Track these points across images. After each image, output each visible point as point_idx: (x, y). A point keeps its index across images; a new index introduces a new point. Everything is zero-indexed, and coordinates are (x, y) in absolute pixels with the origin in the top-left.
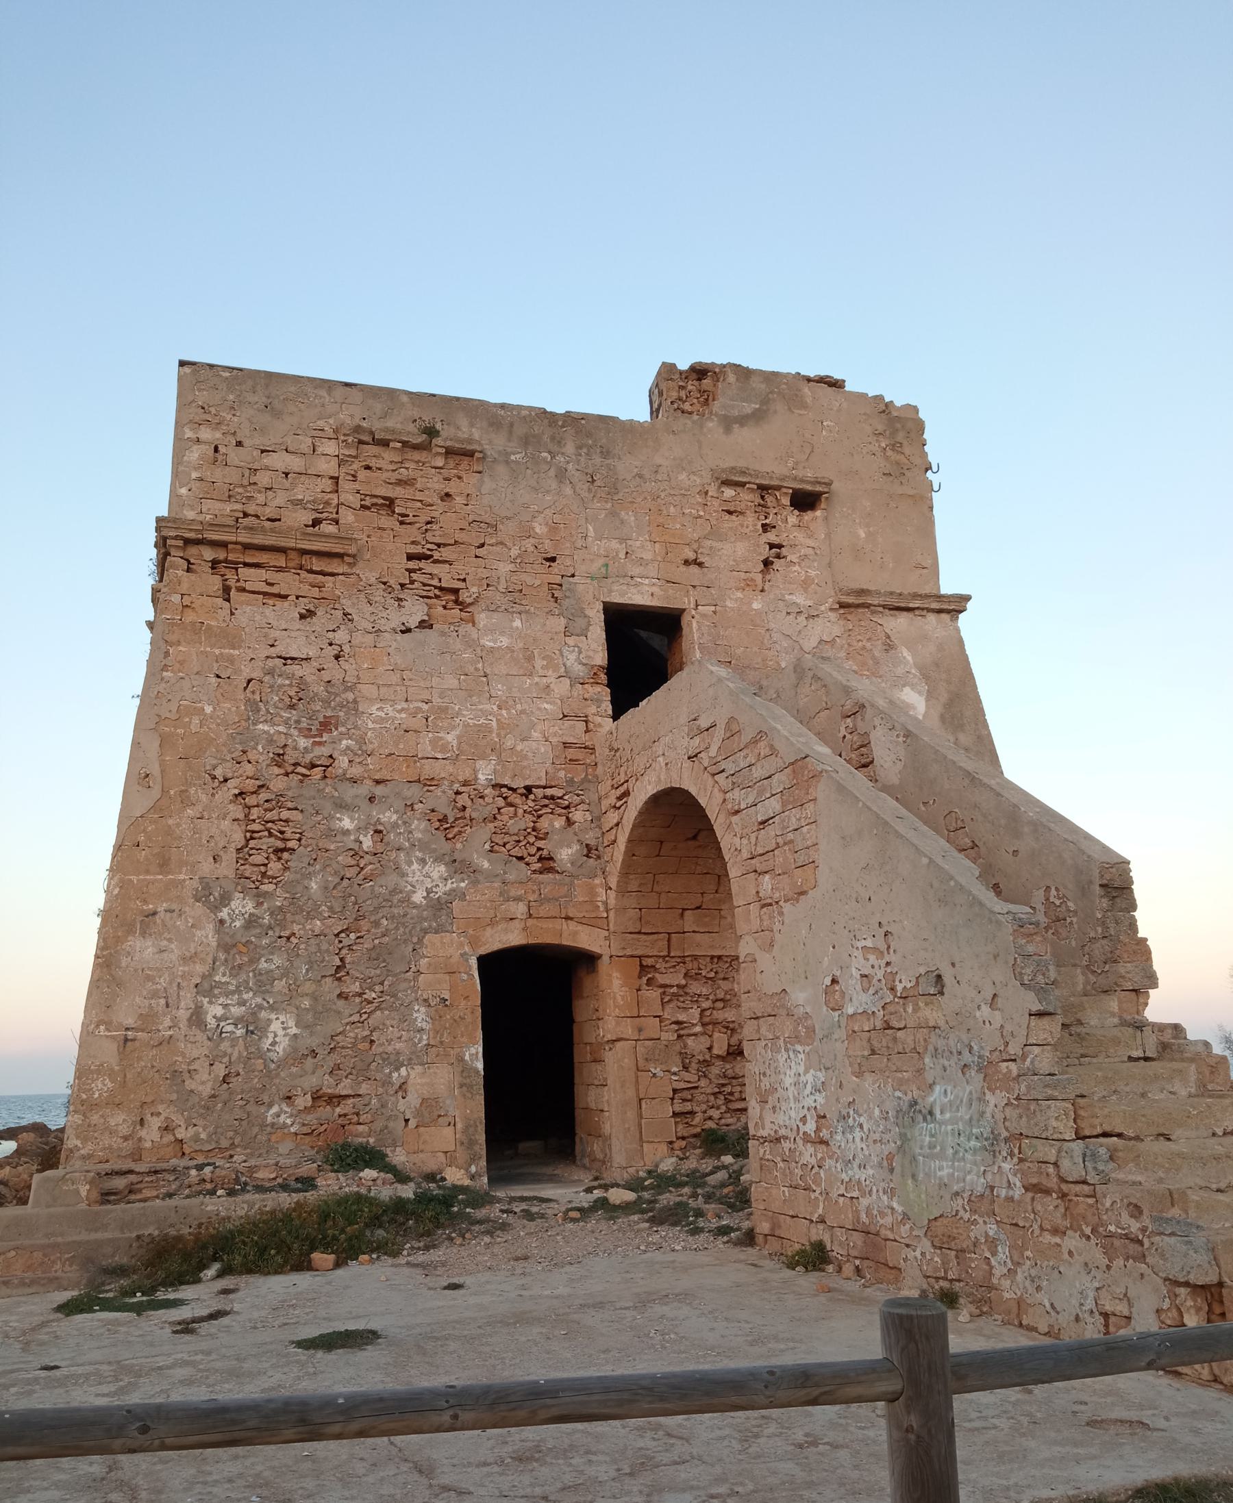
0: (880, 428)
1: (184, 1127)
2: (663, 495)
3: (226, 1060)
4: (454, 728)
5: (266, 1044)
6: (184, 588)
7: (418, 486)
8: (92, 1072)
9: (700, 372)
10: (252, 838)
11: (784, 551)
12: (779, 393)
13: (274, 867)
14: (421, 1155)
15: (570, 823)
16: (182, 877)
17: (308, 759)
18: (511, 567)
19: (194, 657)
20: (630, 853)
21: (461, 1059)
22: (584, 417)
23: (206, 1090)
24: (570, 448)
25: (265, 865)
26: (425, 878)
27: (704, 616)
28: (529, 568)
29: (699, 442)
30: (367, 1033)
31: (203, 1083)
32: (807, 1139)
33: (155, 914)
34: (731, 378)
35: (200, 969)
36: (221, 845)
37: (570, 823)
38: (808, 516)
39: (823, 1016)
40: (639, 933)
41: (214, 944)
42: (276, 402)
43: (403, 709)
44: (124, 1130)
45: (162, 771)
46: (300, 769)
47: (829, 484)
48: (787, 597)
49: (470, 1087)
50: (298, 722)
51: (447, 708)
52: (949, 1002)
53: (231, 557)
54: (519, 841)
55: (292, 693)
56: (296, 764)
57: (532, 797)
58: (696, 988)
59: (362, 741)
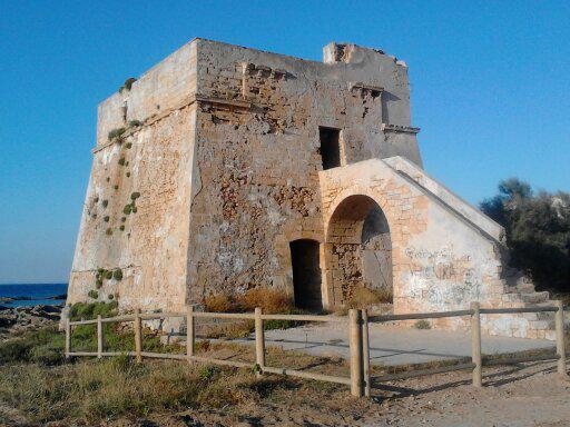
26: (273, 216)
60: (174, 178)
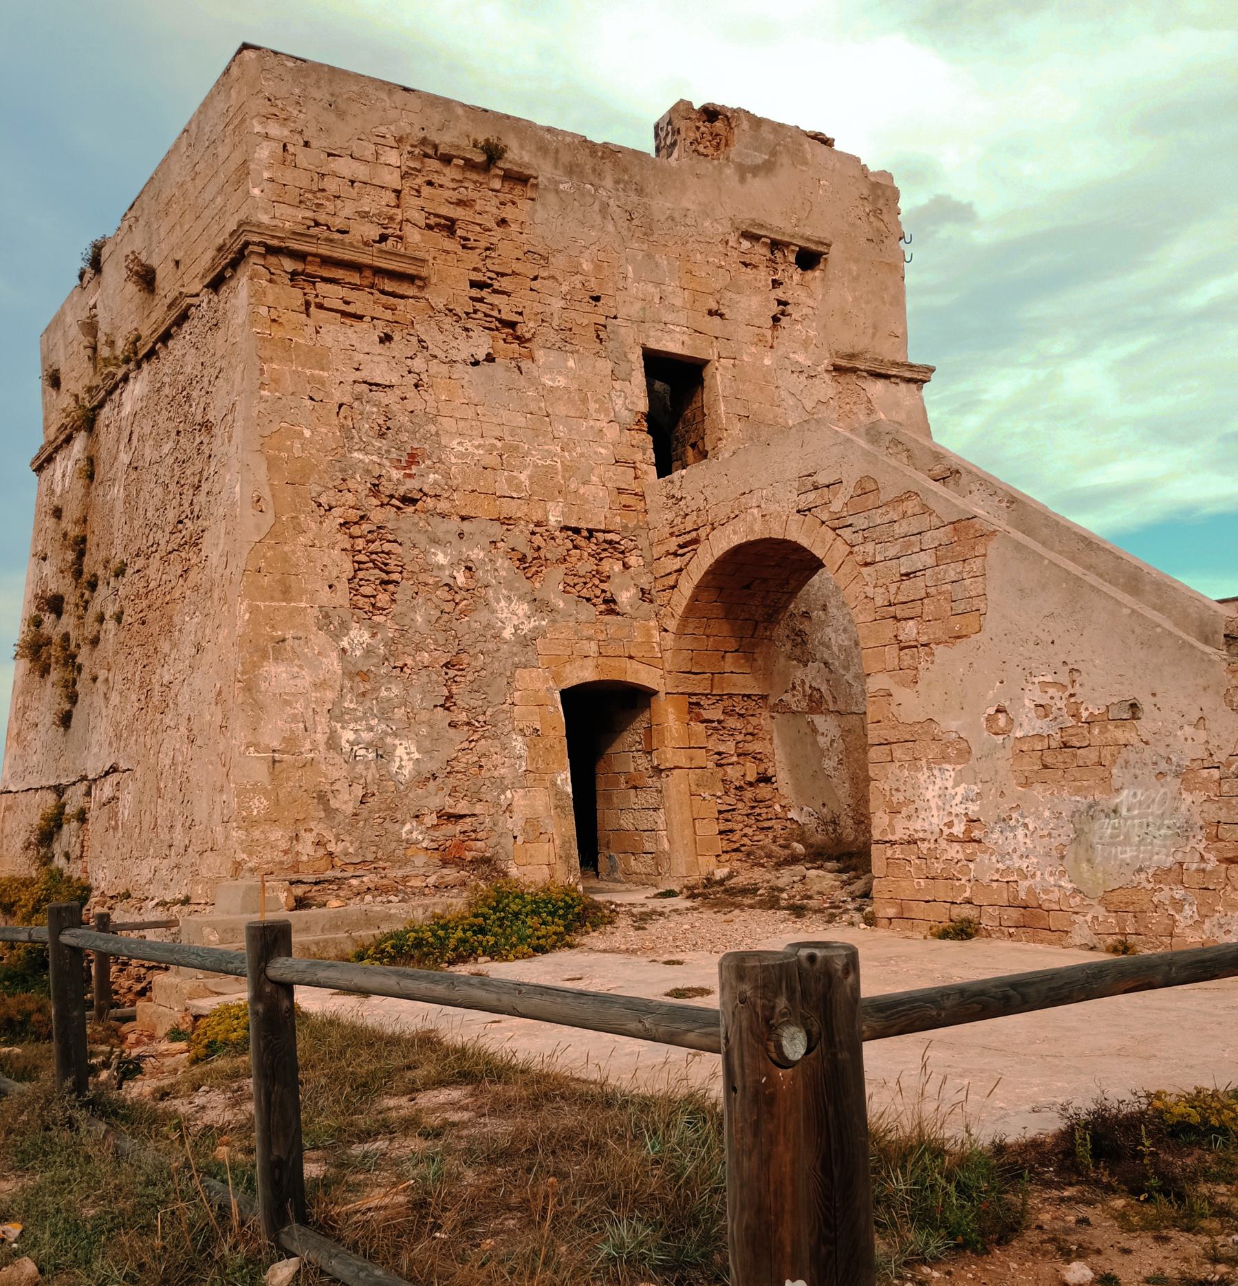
0: (866, 192)
1: (334, 842)
2: (691, 240)
3: (362, 781)
4: (525, 467)
5: (394, 767)
6: (270, 299)
7: (478, 208)
8: (248, 791)
9: (711, 113)
10: (360, 569)
11: (789, 309)
12: (785, 146)
13: (383, 599)
14: (530, 867)
15: (626, 567)
16: (303, 605)
17: (402, 491)
18: (562, 303)
19: (288, 376)
20: (694, 598)
21: (554, 784)
22: (621, 150)
23: (349, 809)
24: (608, 182)
25: (374, 597)
26: (512, 615)
27: (725, 368)
28: (577, 306)
29: (719, 188)
30: (476, 759)
31: (345, 802)
32: (952, 839)
33: (284, 641)
34: (745, 125)
35: (330, 695)
36: (335, 574)
37: (626, 567)
38: (810, 274)
39: (981, 739)
40: (689, 672)
41: (340, 672)
42: (339, 101)
43: (480, 445)
44: (284, 845)
45: (273, 496)
46: (394, 502)
47: (828, 245)
48: (791, 355)
49: (563, 808)
50: (388, 451)
51: (518, 447)
52: (1145, 725)
53: (309, 269)
54: (585, 583)
55: (381, 422)
56: (392, 496)
57: (593, 540)
58: (732, 723)
59: (447, 476)
60: (201, 498)
